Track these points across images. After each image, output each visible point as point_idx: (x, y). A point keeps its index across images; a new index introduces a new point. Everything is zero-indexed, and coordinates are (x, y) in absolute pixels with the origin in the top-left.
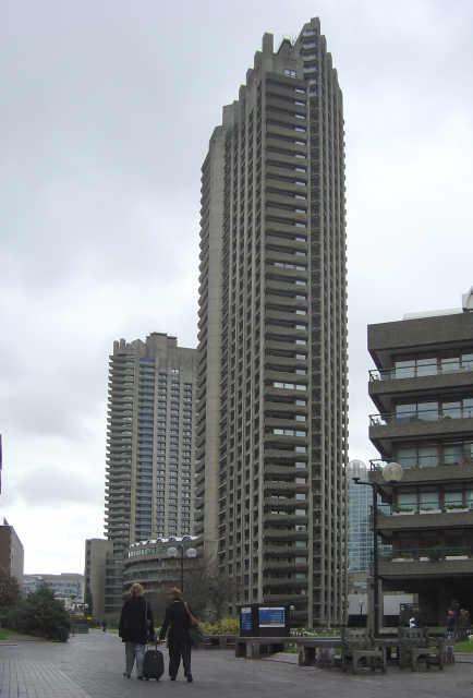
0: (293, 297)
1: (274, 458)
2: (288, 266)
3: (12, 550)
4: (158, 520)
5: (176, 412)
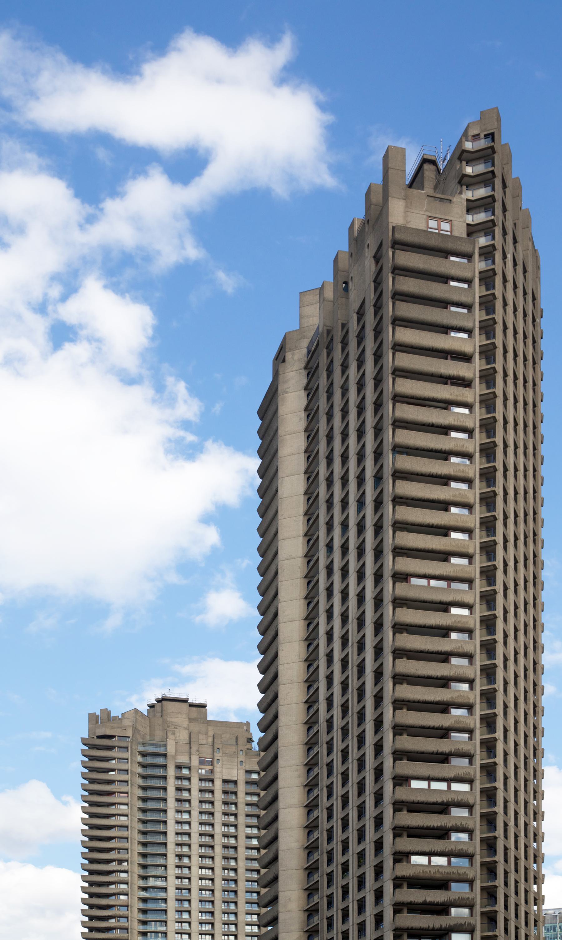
2: (433, 583)
4: (180, 857)
5: (208, 829)
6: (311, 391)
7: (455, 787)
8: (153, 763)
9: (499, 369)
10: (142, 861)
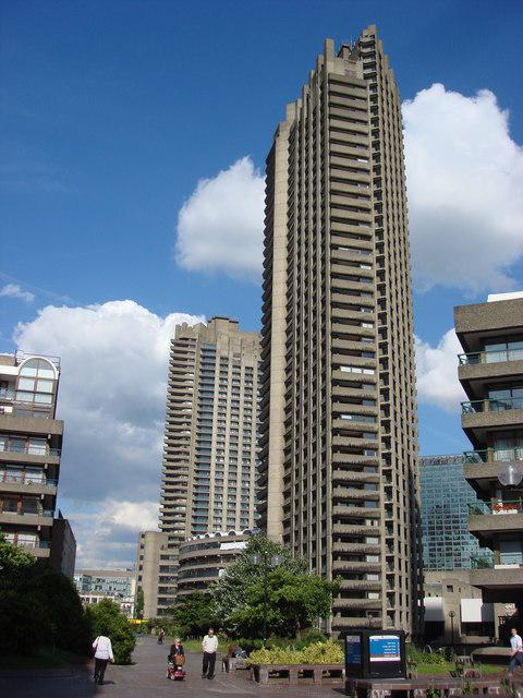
0: (359, 325)
1: (342, 446)
3: (66, 546)
6: (291, 150)
7: (366, 371)
8: (208, 354)
9: (384, 190)
10: (194, 514)
